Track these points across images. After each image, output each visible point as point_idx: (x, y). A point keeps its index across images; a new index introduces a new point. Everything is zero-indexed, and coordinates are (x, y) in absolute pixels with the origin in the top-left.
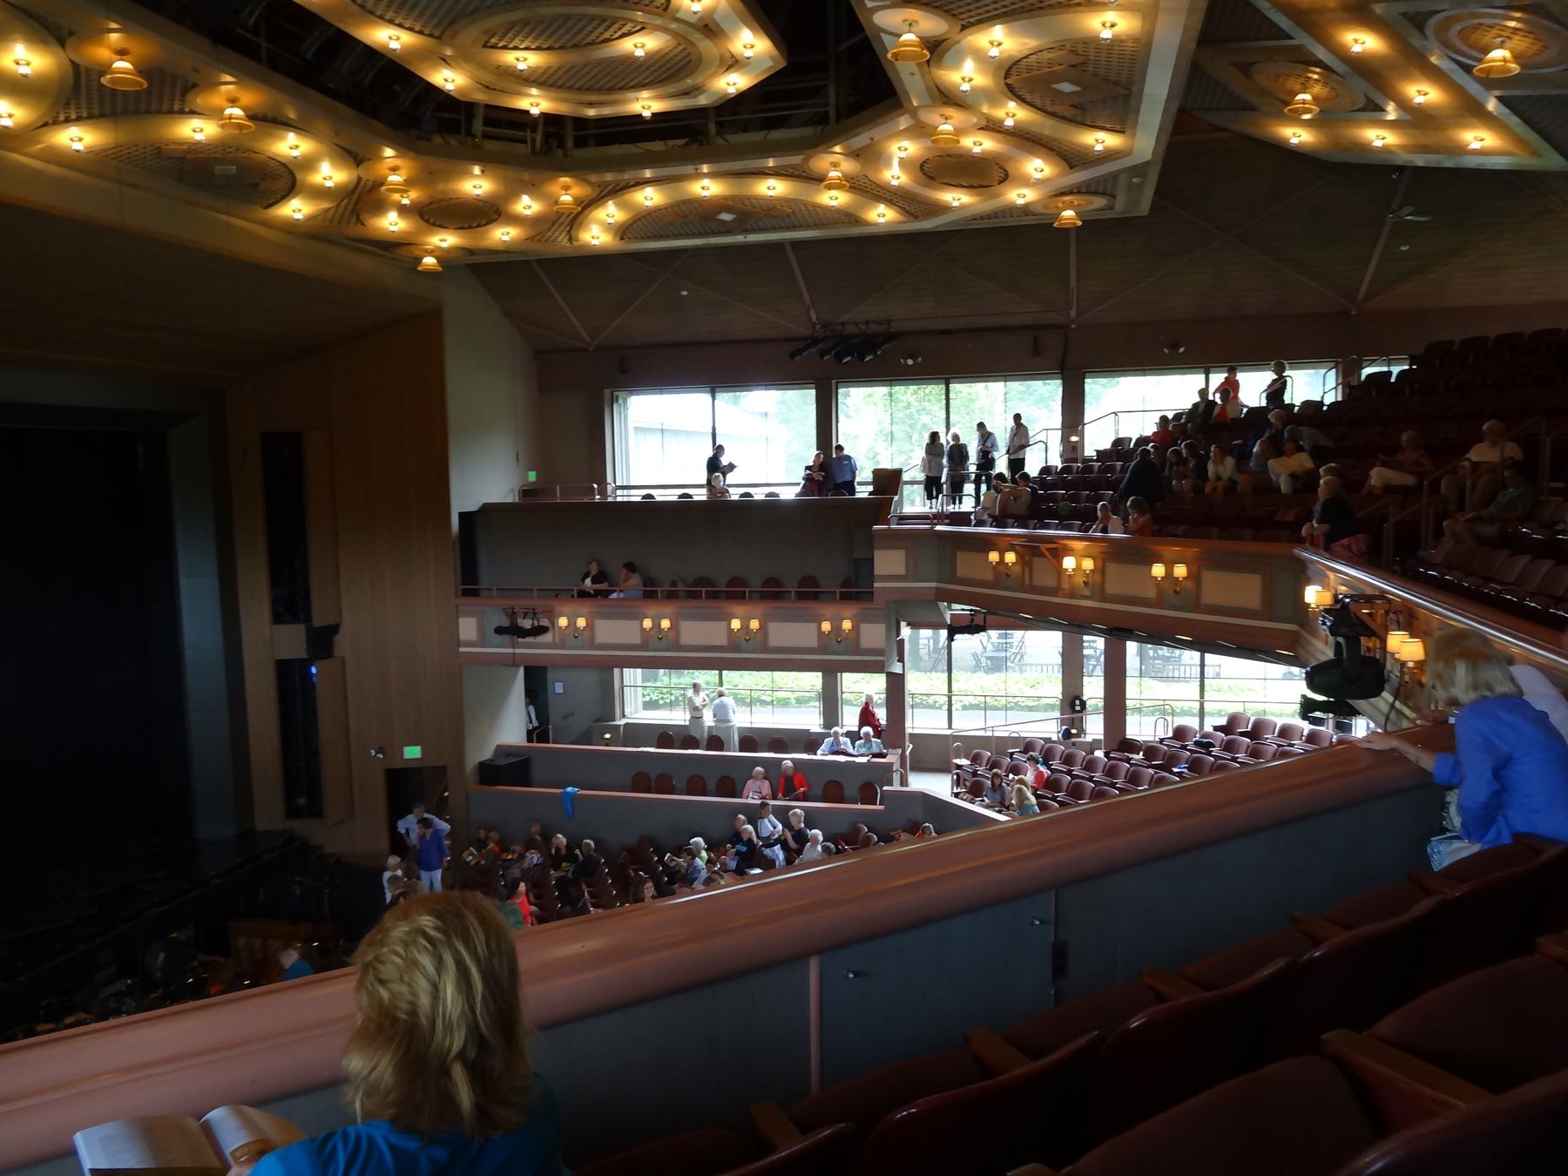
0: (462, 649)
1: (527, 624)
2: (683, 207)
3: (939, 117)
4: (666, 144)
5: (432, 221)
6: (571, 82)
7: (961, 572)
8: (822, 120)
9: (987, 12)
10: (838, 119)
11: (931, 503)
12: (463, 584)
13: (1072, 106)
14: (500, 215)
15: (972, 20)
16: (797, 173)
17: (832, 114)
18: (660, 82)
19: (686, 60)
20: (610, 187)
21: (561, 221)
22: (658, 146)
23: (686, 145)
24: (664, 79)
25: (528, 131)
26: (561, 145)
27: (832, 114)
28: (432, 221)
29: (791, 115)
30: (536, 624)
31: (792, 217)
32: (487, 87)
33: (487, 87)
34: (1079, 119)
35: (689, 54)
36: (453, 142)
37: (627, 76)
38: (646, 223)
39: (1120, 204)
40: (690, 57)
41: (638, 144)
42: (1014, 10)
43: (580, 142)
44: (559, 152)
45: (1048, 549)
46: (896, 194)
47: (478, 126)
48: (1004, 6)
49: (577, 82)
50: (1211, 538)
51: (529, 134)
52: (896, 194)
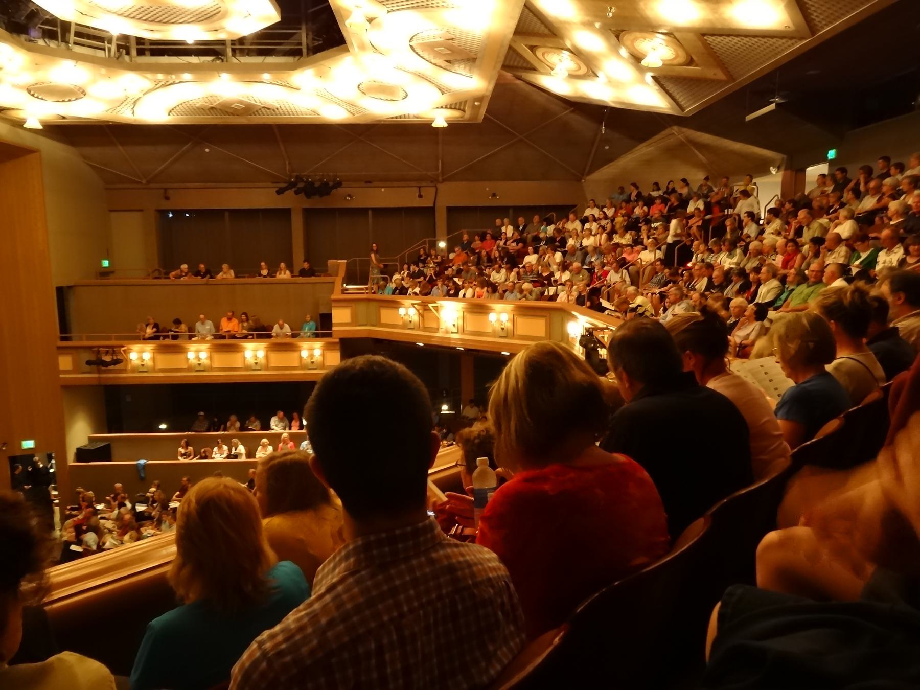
0: (62, 376)
1: (108, 359)
2: (210, 99)
3: (754, 208)
4: (199, 59)
5: (36, 95)
6: (141, 15)
7: (383, 321)
8: (296, 53)
9: (403, 5)
10: (308, 54)
11: (745, 265)
12: (61, 334)
13: (447, 61)
14: (85, 95)
15: (394, 9)
16: (283, 84)
17: (305, 51)
18: (199, 22)
19: (217, 11)
20: (163, 83)
21: (127, 101)
22: (194, 60)
23: (213, 60)
24: (203, 20)
25: (106, 42)
26: (128, 53)
27: (305, 51)
28: (36, 95)
29: (274, 49)
30: (115, 358)
31: (280, 109)
32: (82, 13)
33: (82, 13)
34: (448, 68)
35: (220, 7)
36: (53, 44)
37: (178, 16)
38: (185, 107)
39: (468, 114)
40: (220, 9)
41: (180, 57)
42: (418, 6)
43: (141, 52)
44: (127, 58)
45: (433, 306)
46: (342, 101)
47: (72, 38)
48: (412, 4)
49: (144, 16)
50: (140, 340)
51: (107, 45)
52: (342, 101)
